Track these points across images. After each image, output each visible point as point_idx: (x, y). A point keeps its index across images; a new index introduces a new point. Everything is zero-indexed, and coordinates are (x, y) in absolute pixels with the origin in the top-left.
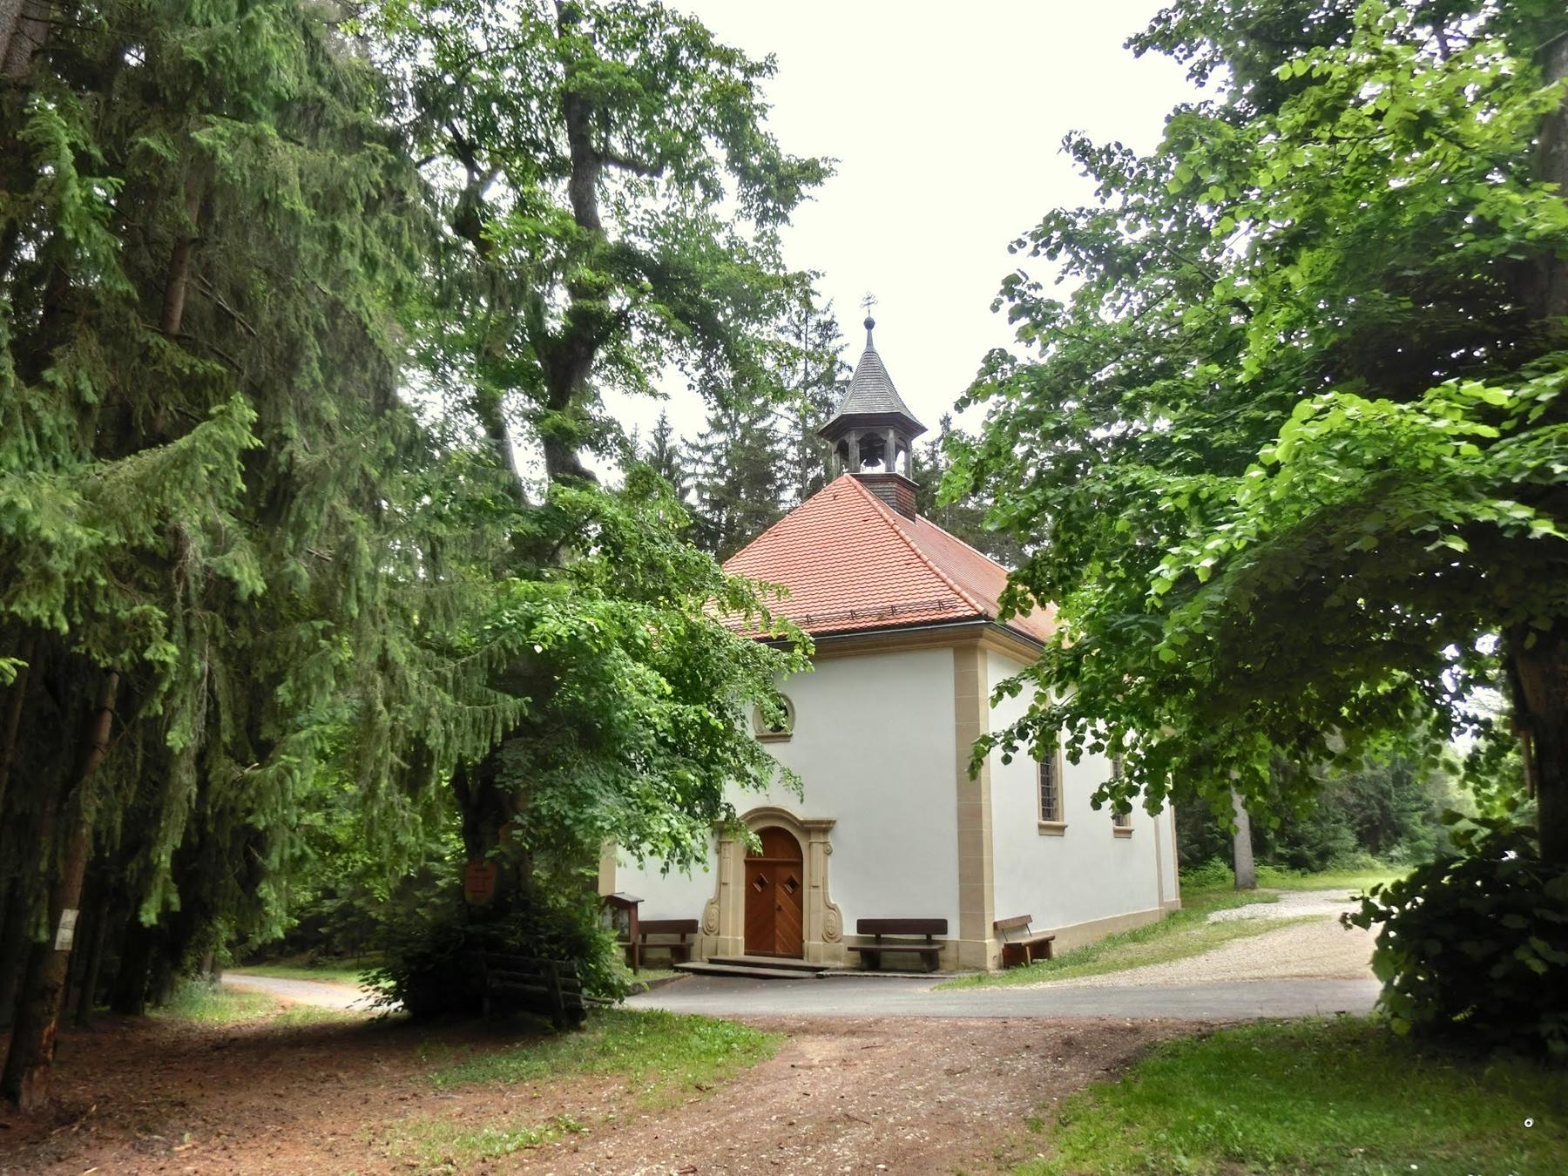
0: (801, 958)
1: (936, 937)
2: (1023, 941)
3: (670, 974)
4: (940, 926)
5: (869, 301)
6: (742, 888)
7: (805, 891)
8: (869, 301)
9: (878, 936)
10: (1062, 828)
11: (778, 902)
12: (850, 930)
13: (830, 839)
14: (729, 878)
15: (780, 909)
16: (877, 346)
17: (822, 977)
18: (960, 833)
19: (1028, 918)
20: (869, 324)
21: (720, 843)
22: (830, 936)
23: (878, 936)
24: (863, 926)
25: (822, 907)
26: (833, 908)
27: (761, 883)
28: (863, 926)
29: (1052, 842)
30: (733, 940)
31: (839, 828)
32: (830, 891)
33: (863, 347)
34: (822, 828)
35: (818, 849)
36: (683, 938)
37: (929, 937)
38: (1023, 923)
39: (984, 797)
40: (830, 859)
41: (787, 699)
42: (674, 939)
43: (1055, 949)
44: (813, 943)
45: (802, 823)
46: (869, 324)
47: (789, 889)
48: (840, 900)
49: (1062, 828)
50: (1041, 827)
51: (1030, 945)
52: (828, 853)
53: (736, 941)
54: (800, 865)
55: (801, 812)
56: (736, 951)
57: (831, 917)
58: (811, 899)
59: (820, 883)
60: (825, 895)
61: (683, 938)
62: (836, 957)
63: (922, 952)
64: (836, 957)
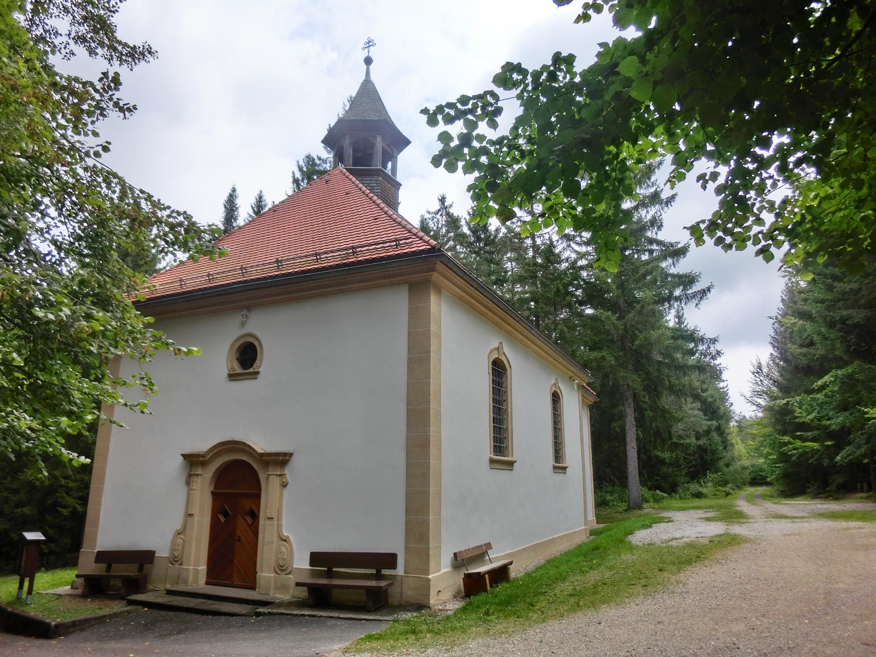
0: (253, 588)
1: (385, 572)
2: (482, 569)
3: (117, 607)
4: (390, 560)
5: (369, 44)
6: (207, 520)
7: (261, 522)
8: (369, 44)
9: (330, 569)
10: (511, 464)
11: (239, 533)
12: (301, 562)
13: (287, 471)
14: (195, 510)
15: (239, 540)
16: (373, 78)
17: (258, 614)
18: (408, 464)
19: (489, 546)
20: (368, 61)
21: (190, 476)
22: (282, 568)
23: (330, 569)
24: (316, 558)
25: (275, 539)
26: (285, 540)
27: (226, 514)
28: (316, 558)
29: (502, 475)
30: (196, 571)
31: (295, 461)
32: (284, 522)
33: (362, 78)
34: (281, 460)
35: (275, 482)
36: (141, 568)
37: (379, 571)
38: (480, 554)
39: (432, 428)
40: (286, 492)
41: (257, 339)
42: (130, 570)
43: (514, 572)
44: (265, 574)
45: (262, 455)
46: (368, 61)
47: (250, 521)
48: (295, 533)
49: (511, 464)
50: (492, 461)
51: (489, 572)
52: (284, 485)
53: (196, 572)
54: (258, 496)
55: (261, 444)
56: (196, 580)
57: (283, 549)
58: (266, 533)
59: (274, 515)
60: (279, 526)
61: (141, 568)
62: (283, 588)
63: (368, 589)
64: (283, 588)
